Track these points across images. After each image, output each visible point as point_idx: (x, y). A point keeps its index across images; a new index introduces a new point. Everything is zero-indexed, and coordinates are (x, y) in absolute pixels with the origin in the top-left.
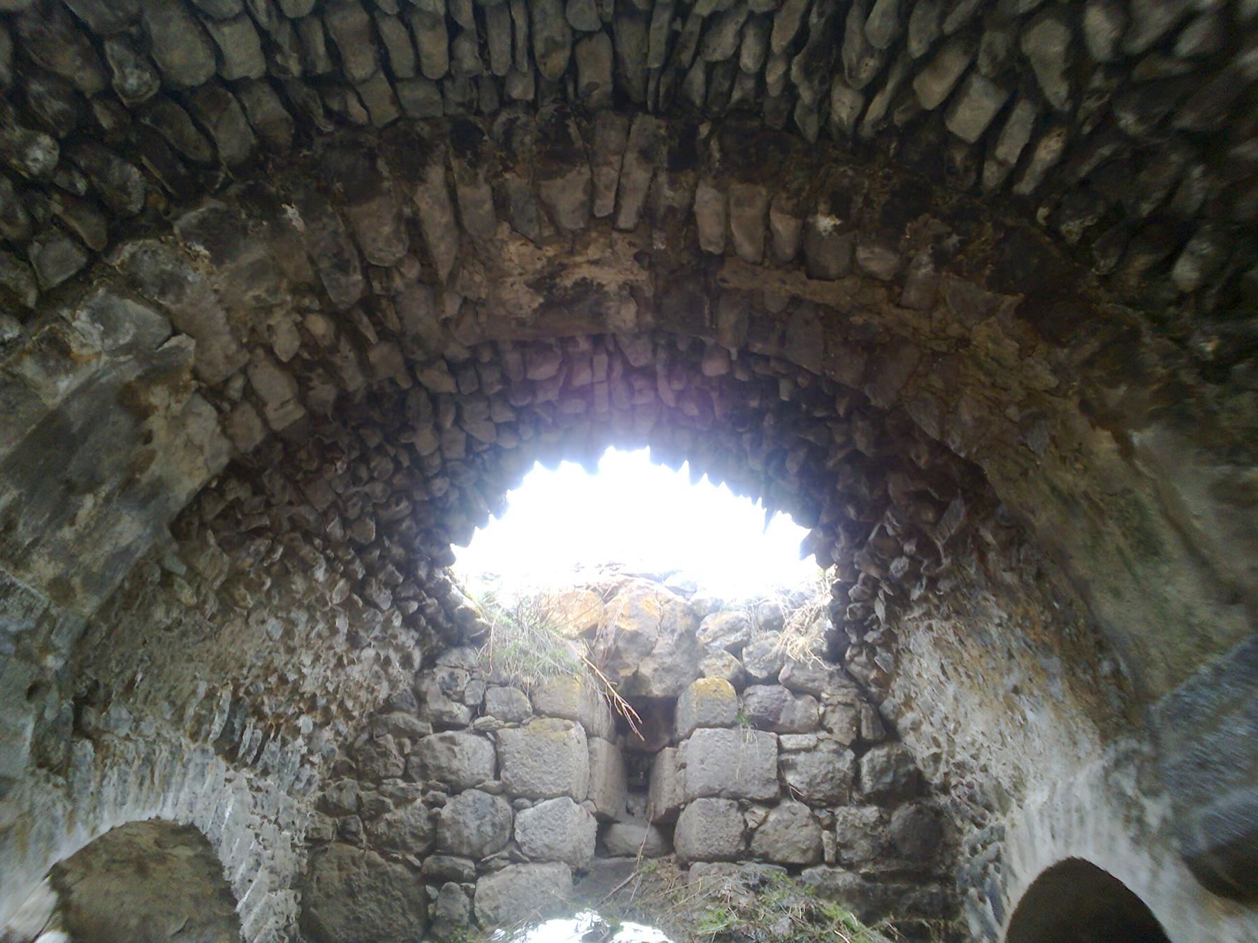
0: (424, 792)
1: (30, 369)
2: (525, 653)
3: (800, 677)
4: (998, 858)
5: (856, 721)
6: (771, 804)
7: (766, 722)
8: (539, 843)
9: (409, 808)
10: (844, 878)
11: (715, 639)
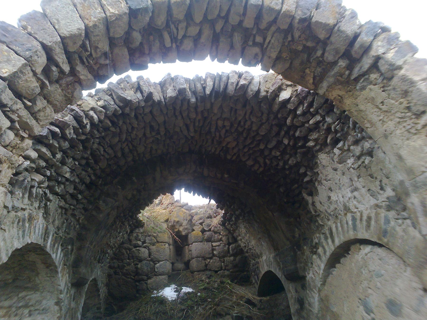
0: (133, 262)
1: (94, 213)
2: (153, 228)
3: (216, 229)
4: (258, 268)
5: (228, 239)
6: (211, 258)
7: (209, 240)
8: (161, 271)
9: (131, 266)
10: (227, 273)
11: (196, 222)
